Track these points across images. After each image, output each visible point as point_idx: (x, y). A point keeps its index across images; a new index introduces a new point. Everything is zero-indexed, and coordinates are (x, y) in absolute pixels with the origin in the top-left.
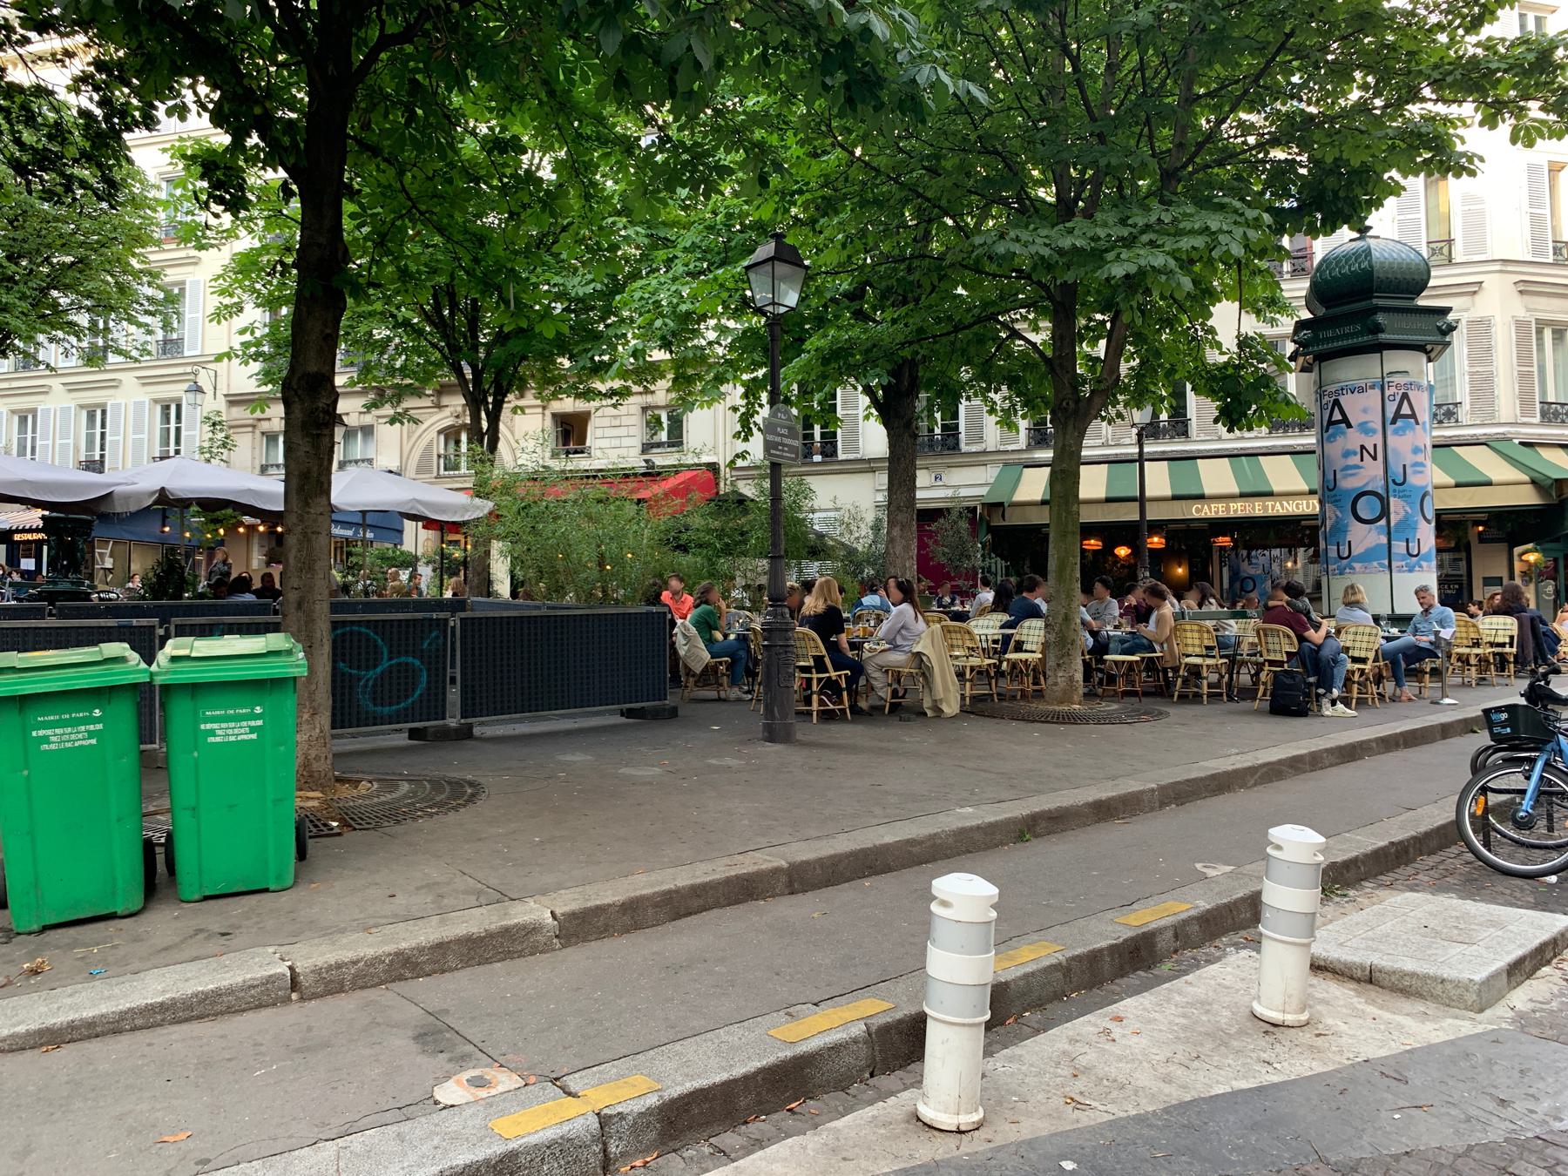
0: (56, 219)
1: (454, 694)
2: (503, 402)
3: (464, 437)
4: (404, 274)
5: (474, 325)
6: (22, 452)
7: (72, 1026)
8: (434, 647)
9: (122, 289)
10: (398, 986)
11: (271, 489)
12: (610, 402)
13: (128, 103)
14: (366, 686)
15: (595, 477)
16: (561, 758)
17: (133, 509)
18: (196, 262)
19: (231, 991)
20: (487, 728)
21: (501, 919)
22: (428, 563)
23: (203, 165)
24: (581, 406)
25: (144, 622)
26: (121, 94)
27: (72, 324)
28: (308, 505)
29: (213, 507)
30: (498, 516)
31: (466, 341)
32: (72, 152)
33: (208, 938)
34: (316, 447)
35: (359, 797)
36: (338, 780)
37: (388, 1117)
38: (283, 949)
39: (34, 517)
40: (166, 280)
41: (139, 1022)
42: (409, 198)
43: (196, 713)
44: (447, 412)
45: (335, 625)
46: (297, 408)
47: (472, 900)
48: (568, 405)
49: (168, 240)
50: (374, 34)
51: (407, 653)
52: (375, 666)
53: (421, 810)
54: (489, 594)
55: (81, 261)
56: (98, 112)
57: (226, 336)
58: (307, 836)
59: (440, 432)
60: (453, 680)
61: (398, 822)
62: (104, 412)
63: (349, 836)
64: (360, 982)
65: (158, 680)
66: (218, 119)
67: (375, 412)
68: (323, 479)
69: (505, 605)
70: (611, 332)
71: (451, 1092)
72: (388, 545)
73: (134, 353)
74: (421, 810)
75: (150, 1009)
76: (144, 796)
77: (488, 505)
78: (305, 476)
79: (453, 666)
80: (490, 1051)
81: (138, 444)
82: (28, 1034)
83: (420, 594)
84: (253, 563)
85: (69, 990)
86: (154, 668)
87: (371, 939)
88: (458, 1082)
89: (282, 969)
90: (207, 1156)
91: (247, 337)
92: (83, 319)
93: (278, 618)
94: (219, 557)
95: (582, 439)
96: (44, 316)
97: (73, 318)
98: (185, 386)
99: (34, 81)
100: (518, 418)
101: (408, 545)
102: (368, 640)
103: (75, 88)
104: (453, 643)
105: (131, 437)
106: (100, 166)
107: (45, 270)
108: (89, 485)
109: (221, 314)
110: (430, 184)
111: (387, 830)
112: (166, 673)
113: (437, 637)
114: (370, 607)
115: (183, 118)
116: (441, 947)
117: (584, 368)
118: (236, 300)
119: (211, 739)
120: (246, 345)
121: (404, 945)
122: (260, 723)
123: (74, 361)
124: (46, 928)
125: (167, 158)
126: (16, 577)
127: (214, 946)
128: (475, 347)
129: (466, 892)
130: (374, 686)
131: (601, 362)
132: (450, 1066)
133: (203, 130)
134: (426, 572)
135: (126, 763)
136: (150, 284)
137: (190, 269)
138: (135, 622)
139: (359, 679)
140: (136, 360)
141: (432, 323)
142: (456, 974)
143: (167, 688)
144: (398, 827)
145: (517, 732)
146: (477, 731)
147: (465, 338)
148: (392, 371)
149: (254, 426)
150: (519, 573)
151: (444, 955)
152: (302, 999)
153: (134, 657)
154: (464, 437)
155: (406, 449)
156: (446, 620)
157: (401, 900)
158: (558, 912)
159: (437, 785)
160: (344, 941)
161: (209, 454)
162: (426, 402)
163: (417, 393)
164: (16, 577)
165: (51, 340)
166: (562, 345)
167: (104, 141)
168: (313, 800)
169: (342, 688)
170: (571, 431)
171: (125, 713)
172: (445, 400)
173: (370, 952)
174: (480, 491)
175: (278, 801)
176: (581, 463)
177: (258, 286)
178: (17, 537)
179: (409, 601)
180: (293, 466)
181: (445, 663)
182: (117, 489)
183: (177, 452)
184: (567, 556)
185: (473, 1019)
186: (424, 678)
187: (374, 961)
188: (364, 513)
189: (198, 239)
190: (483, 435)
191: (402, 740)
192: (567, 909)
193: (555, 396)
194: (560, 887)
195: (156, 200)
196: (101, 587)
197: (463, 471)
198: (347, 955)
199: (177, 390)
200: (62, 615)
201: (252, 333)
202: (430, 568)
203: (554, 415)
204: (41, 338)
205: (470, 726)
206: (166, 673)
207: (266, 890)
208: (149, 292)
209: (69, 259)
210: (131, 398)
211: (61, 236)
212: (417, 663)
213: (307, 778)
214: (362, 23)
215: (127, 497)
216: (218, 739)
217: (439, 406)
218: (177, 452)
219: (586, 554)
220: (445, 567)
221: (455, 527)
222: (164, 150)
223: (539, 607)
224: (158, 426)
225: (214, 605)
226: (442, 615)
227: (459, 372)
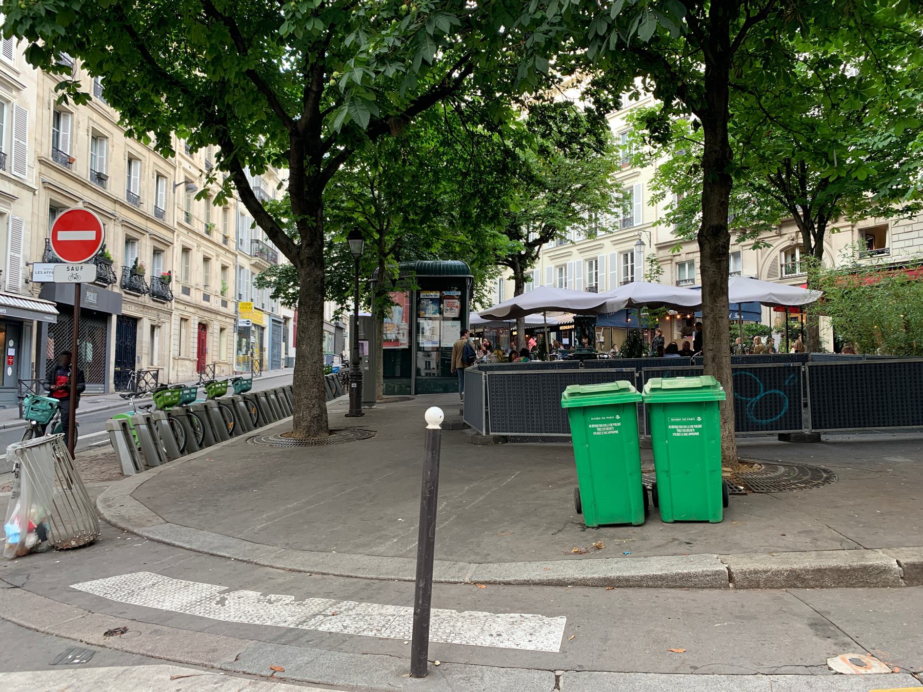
0: (573, 167)
1: (807, 414)
2: (825, 226)
3: (797, 252)
4: (762, 158)
5: (803, 182)
6: (561, 286)
7: (618, 579)
8: (792, 384)
9: (603, 196)
10: (793, 591)
11: (692, 295)
12: (906, 215)
13: (607, 99)
14: (751, 406)
15: (900, 268)
16: (887, 459)
17: (616, 310)
18: (637, 175)
19: (696, 576)
20: (830, 436)
21: (860, 560)
22: (778, 332)
23: (647, 122)
24: (881, 221)
25: (629, 370)
26: (605, 94)
27: (581, 219)
28: (716, 301)
29: (655, 307)
30: (828, 300)
31: (798, 192)
32: (583, 130)
33: (680, 543)
34: (719, 268)
35: (755, 473)
36: (740, 462)
37: (799, 670)
38: (722, 557)
39: (569, 318)
40: (624, 187)
41: (651, 583)
42: (765, 112)
43: (585, 422)
44: (786, 238)
45: (734, 370)
46: (707, 247)
47: (837, 545)
48: (870, 222)
49: (624, 165)
50: (743, 21)
51: (775, 388)
52: (756, 395)
53: (794, 484)
54: (820, 351)
55: (584, 186)
56: (593, 107)
57: (660, 211)
58: (728, 493)
59: (781, 251)
60: (806, 405)
61: (780, 490)
62: (596, 262)
63: (751, 496)
64: (769, 584)
65: (647, 401)
66: (657, 95)
67: (742, 243)
68: (724, 286)
69: (830, 357)
70: (905, 168)
71: (838, 664)
72: (752, 322)
73: (610, 229)
74: (794, 484)
75: (655, 578)
76: (642, 462)
77: (817, 294)
78: (714, 285)
79: (805, 396)
80: (862, 644)
81: (613, 275)
82: (600, 579)
83: (774, 350)
84: (675, 336)
85: (615, 560)
86: (643, 394)
87: (773, 559)
88: (844, 659)
89: (723, 568)
90: (696, 665)
91: (669, 211)
92: (586, 215)
93: (702, 367)
94: (657, 333)
95: (882, 243)
96: (569, 217)
97: (581, 215)
98: (635, 243)
99: (565, 99)
100: (835, 236)
101: (765, 322)
102: (751, 380)
103: (583, 98)
104: (805, 383)
105: (609, 273)
106: (595, 135)
107: (569, 193)
108: (590, 300)
109: (653, 201)
110: (777, 100)
111: (774, 494)
112: (650, 397)
113: (794, 378)
114: (749, 360)
115: (637, 99)
116: (819, 571)
117: (885, 196)
118: (661, 191)
119: (674, 434)
120: (668, 215)
121: (795, 566)
122: (700, 426)
123: (582, 237)
124: (600, 526)
125: (624, 122)
126: (562, 348)
127: (684, 548)
128: (804, 195)
129: (833, 539)
130: (756, 407)
131: (897, 189)
132: (835, 648)
133: (651, 103)
134: (777, 339)
135: (632, 445)
136: (616, 191)
137: (635, 179)
138: (624, 370)
139: (747, 403)
140: (611, 232)
141: (776, 185)
142: (831, 590)
143: (650, 405)
144: (780, 493)
145: (851, 440)
146: (823, 438)
147: (797, 190)
148: (753, 218)
149: (671, 260)
150: (840, 337)
151: (822, 577)
152: (735, 587)
153: (633, 389)
154: (797, 252)
155: (761, 263)
156: (799, 367)
157: (790, 538)
158: (902, 561)
159: (802, 470)
160: (757, 558)
161: (650, 278)
162: (773, 233)
163: (767, 228)
164: (562, 348)
165: (573, 228)
166: (868, 184)
167: (596, 120)
168: (728, 472)
169: (739, 406)
170: (874, 239)
171: (630, 417)
172: (784, 231)
173: (775, 567)
174: (811, 284)
175: (712, 472)
176: (886, 260)
177: (673, 181)
178: (561, 328)
179: (768, 356)
180: (706, 279)
181: (800, 394)
182: (608, 301)
183: (632, 278)
184: (880, 323)
185: (847, 621)
186: (787, 403)
187: (777, 573)
188: (740, 304)
189: (641, 162)
190: (812, 250)
191: (774, 440)
192: (909, 560)
193: (861, 217)
194: (899, 545)
195: (618, 146)
196: (600, 352)
197: (798, 272)
198: (761, 567)
199: (631, 245)
200: (586, 367)
201: (671, 208)
202: (780, 335)
203: (860, 230)
204: (568, 228)
205: (819, 434)
206: (650, 397)
207: (708, 522)
208: (616, 195)
209: (579, 186)
210: (609, 252)
211: (575, 175)
212: (782, 393)
213: (726, 461)
214: (736, 15)
215: (613, 304)
216: (678, 434)
217: (780, 235)
218: (632, 278)
219: (896, 321)
220: (789, 334)
221: (799, 309)
222: (623, 118)
223: (856, 356)
224: (622, 265)
225: (659, 360)
226: (796, 364)
227: (795, 212)
